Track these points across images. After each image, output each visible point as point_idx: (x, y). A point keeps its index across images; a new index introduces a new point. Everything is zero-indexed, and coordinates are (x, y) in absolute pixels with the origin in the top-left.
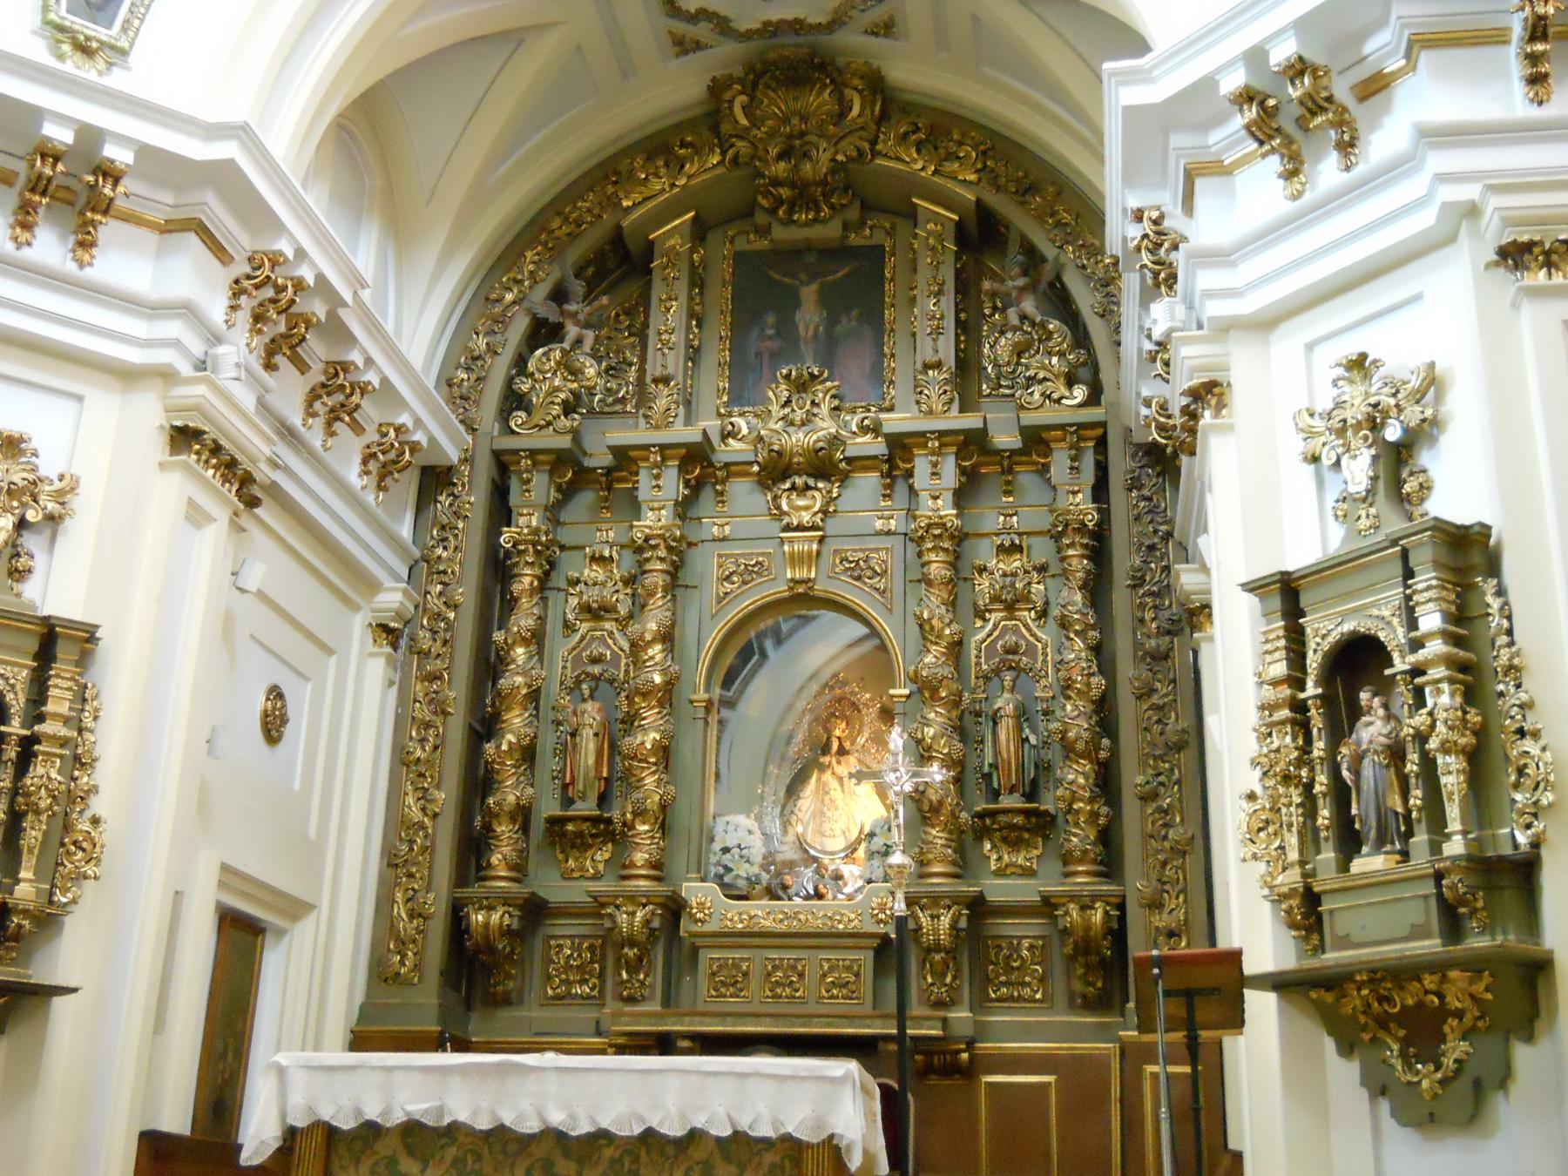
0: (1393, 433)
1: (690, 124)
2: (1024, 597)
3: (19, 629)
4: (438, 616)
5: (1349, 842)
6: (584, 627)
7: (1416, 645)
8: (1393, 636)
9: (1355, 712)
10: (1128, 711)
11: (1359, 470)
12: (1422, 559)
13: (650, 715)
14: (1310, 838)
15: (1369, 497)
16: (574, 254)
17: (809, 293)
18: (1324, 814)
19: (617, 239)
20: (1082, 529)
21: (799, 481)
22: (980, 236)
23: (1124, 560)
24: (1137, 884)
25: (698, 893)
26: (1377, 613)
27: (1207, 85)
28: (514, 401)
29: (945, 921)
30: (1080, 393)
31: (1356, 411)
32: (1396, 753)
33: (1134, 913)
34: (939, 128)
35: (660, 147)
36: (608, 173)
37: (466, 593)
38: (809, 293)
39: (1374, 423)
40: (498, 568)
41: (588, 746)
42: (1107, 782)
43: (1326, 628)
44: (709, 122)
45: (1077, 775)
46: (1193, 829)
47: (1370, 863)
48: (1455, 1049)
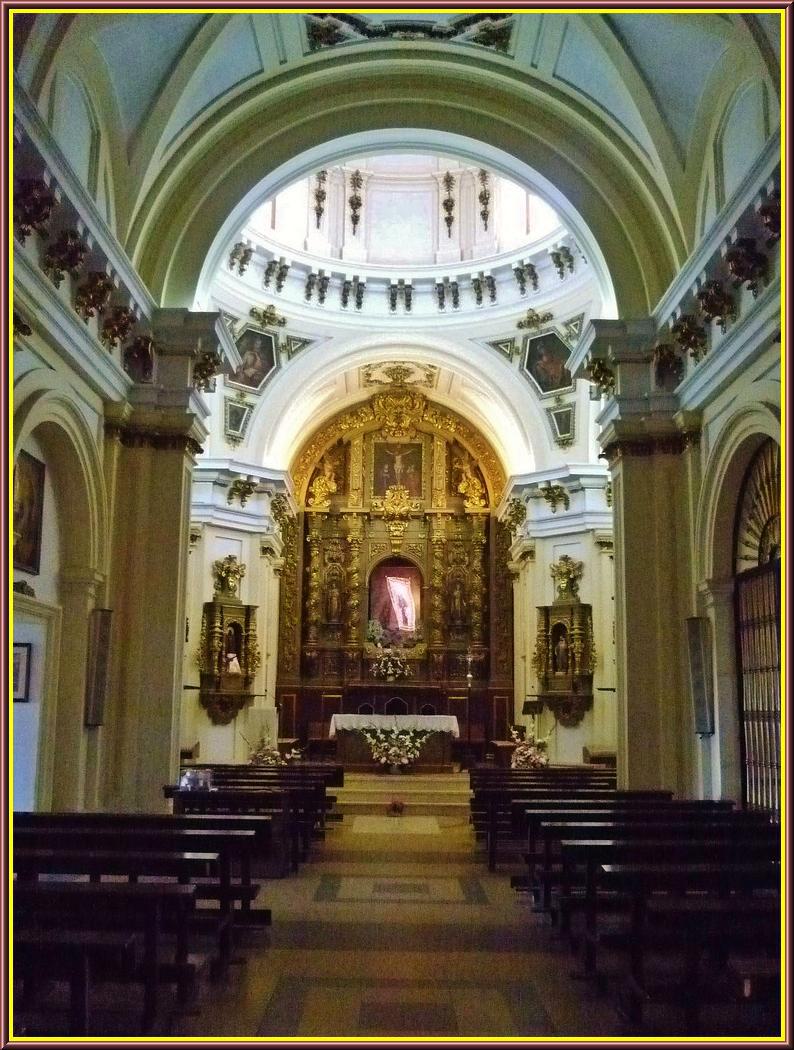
0: (571, 576)
1: (365, 402)
2: (463, 561)
3: (601, 775)
4: (292, 565)
5: (555, 669)
6: (330, 564)
7: (573, 629)
8: (568, 626)
9: (559, 640)
10: (493, 598)
11: (563, 583)
12: (575, 611)
13: (355, 595)
14: (547, 667)
15: (565, 591)
16: (328, 446)
17: (398, 458)
18: (550, 662)
19: (340, 441)
20: (482, 544)
21: (397, 522)
22: (453, 447)
23: (493, 557)
24: (494, 647)
25: (369, 646)
26: (565, 621)
27: (510, 265)
28: (310, 495)
29: (441, 657)
30: (483, 503)
31: (564, 570)
32: (567, 650)
33: (493, 657)
34: (444, 412)
35: (353, 411)
36: (335, 420)
37: (299, 557)
38: (398, 458)
39: (569, 572)
40: (307, 548)
41: (335, 602)
42: (486, 617)
43: (554, 621)
44: (370, 402)
45: (476, 616)
46: (510, 635)
47: (559, 673)
48: (574, 712)
